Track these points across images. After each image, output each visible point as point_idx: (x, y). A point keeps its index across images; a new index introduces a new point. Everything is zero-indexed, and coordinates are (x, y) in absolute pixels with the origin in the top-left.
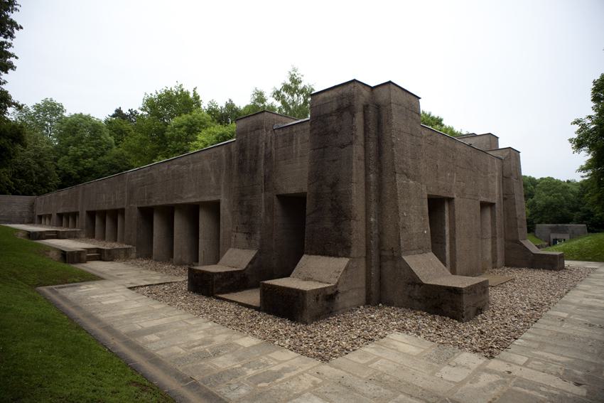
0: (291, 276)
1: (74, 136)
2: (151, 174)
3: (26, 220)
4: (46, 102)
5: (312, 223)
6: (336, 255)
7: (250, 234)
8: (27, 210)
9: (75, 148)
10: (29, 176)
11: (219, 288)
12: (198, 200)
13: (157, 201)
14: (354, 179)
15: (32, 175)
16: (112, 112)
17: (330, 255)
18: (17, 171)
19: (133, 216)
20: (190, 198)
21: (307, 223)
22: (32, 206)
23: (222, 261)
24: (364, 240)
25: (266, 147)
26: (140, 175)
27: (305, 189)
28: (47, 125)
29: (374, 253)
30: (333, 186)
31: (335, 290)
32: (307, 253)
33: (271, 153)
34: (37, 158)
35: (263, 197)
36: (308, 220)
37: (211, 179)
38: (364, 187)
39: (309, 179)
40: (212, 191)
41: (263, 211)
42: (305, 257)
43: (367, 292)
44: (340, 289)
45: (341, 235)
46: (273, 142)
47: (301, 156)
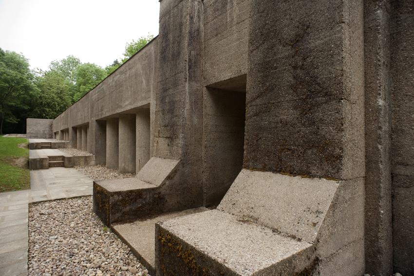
0: (219, 207)
1: (84, 78)
2: (103, 88)
3: (47, 136)
4: (69, 58)
5: (256, 115)
6: (306, 173)
7: (171, 138)
8: (47, 129)
9: (84, 87)
10: (54, 106)
11: (118, 215)
12: (132, 107)
13: (107, 113)
14: (346, 17)
15: (55, 106)
16: (112, 63)
17: (292, 173)
18: (46, 103)
19: (93, 128)
20: (127, 105)
21: (247, 116)
22: (51, 126)
23: (140, 174)
24: (362, 144)
25: (192, 23)
26: (97, 92)
27: (245, 70)
28: (70, 73)
29: (384, 168)
30: (297, 41)
31: (313, 257)
32: (247, 168)
33: (198, 30)
34: (58, 94)
35: (187, 88)
36: (249, 111)
37: (142, 82)
38: (362, 38)
39: (251, 42)
40: (143, 95)
41: (188, 106)
42: (244, 174)
43: (367, 248)
44: (323, 252)
45: (316, 133)
46: (202, 17)
47: (238, 23)
